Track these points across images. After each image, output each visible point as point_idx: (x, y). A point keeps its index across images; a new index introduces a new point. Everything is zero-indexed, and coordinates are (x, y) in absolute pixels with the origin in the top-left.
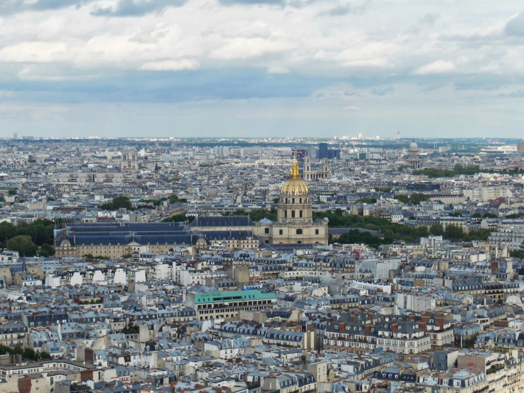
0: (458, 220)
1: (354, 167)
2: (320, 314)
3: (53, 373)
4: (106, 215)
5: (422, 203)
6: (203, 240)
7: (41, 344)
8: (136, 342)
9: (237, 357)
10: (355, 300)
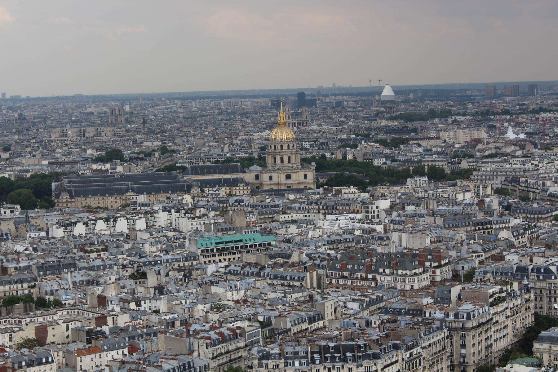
1: (332, 115)
2: (320, 254)
4: (100, 167)
5: (402, 146)
6: (197, 188)
7: (52, 292)
9: (243, 299)
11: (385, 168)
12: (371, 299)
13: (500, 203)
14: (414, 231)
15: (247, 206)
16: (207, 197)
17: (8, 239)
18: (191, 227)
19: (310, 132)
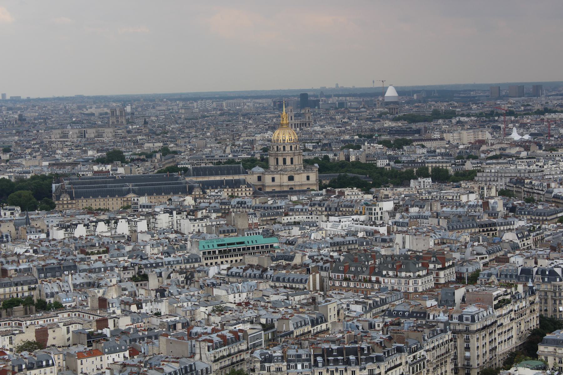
1: (335, 116)
2: (323, 257)
4: (101, 168)
5: (405, 148)
6: (199, 189)
7: (52, 295)
9: (245, 301)
11: (388, 169)
12: (374, 301)
13: (505, 205)
14: (418, 233)
15: (249, 208)
16: (209, 199)
17: (8, 241)
18: (192, 228)
19: (313, 133)
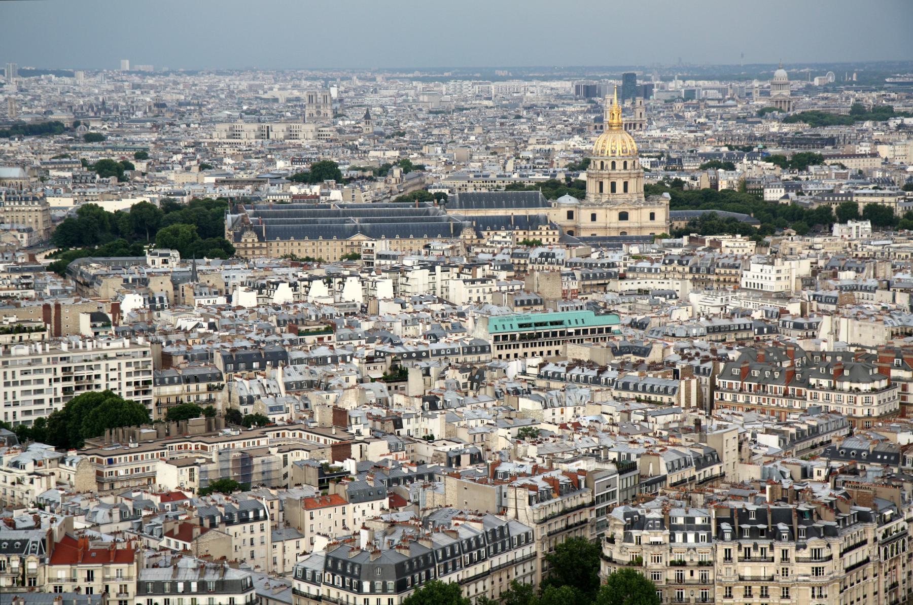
0: (883, 195)
1: (683, 112)
3: (287, 448)
4: (303, 191)
5: (812, 168)
7: (251, 400)
8: (405, 395)
9: (573, 421)
10: (748, 327)
12: (798, 429)
14: (862, 316)
17: (162, 308)
